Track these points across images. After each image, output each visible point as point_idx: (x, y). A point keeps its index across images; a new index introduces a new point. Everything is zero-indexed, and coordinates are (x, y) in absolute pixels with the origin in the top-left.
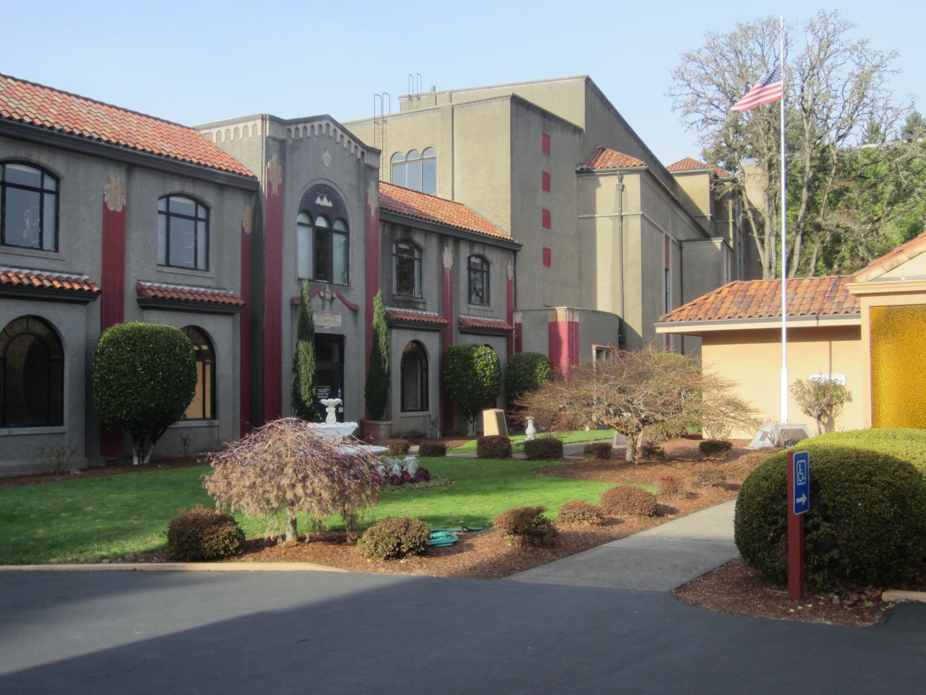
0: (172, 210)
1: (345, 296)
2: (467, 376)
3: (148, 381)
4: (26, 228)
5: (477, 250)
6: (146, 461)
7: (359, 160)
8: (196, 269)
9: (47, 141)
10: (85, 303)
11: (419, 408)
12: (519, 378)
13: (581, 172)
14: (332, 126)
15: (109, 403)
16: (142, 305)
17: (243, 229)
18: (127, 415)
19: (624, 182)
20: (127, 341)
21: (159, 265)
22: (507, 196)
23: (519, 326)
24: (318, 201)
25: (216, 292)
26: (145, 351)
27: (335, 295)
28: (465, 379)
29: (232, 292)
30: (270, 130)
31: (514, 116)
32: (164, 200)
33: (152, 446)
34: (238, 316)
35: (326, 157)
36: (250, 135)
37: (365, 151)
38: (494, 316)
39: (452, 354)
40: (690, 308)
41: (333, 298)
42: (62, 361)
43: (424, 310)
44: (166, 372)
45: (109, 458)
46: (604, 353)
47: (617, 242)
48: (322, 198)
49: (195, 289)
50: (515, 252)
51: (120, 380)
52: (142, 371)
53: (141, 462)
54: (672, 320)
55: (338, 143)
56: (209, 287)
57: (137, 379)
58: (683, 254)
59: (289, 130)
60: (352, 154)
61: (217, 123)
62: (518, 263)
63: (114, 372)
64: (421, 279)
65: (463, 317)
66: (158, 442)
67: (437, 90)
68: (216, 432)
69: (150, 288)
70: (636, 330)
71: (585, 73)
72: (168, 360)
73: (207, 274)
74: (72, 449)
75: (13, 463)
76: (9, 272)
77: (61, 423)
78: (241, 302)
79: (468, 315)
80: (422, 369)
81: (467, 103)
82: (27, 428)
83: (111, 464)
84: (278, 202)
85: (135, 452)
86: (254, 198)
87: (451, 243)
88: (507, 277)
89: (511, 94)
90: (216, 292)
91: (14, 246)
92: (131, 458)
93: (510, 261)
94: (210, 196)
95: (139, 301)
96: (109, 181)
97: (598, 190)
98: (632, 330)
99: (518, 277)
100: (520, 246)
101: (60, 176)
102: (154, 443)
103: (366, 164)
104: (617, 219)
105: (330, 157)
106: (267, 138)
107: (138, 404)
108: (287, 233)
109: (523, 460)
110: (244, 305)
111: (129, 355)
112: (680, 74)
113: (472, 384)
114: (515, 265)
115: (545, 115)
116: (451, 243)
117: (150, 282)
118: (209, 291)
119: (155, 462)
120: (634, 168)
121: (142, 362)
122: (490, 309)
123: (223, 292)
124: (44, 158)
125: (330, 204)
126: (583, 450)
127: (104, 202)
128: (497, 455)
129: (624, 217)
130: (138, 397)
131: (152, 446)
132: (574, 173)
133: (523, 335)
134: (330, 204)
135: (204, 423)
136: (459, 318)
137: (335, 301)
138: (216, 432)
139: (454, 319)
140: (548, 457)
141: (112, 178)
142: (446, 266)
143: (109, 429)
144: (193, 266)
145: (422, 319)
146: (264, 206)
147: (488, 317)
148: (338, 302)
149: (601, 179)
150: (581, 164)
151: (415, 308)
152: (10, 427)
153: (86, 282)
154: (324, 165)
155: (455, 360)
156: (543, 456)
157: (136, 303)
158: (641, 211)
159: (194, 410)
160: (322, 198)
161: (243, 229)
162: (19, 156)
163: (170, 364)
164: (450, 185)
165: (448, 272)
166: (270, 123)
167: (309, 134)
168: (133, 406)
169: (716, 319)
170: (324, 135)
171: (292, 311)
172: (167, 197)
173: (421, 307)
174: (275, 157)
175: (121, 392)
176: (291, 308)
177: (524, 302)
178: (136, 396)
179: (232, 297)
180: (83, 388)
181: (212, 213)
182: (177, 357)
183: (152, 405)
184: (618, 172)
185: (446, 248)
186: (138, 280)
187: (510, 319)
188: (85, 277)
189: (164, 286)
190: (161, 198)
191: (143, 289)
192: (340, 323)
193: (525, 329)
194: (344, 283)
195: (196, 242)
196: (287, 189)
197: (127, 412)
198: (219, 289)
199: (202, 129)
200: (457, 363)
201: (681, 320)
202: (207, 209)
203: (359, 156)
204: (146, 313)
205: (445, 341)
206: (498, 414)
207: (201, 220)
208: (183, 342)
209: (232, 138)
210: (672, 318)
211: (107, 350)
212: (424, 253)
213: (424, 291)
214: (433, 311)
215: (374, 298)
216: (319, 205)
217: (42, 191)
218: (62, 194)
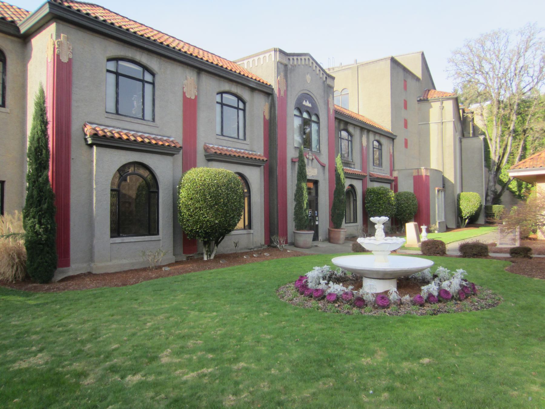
0: (224, 102)
1: (319, 158)
2: (379, 204)
3: (214, 205)
4: (134, 107)
5: (377, 137)
6: (212, 257)
7: (324, 81)
8: (238, 138)
9: (146, 46)
10: (172, 155)
11: (352, 221)
12: (401, 205)
13: (420, 101)
14: (311, 60)
15: (188, 220)
16: (207, 158)
17: (264, 116)
18: (200, 228)
19: (443, 105)
20: (199, 179)
21: (217, 135)
22: (389, 110)
23: (396, 178)
24: (304, 103)
25: (251, 152)
26: (212, 185)
27: (314, 157)
28: (378, 205)
29: (259, 153)
30: (279, 57)
31: (392, 68)
32: (219, 96)
33: (216, 247)
34: (262, 167)
35: (308, 77)
36: (267, 61)
37: (327, 77)
38: (383, 173)
39: (370, 192)
40: (530, 160)
41: (313, 159)
42: (157, 193)
43: (354, 168)
44: (225, 199)
45: (189, 255)
48: (306, 101)
49: (238, 150)
50: (393, 139)
51: (195, 204)
52: (210, 198)
53: (209, 258)
54: (520, 168)
55: (314, 70)
56: (246, 150)
57: (207, 204)
59: (289, 59)
60: (321, 78)
61: (247, 57)
62: (395, 146)
63: (191, 199)
64: (352, 152)
65: (372, 172)
66: (219, 245)
67: (343, 65)
68: (252, 237)
69: (212, 148)
71: (422, 50)
72: (227, 191)
73: (245, 142)
74: (164, 251)
75: (125, 261)
76: (122, 132)
77: (158, 234)
78: (265, 159)
79: (373, 171)
80: (354, 200)
82: (135, 237)
83: (190, 260)
84: (284, 100)
85: (205, 252)
86: (270, 98)
87: (365, 132)
90: (251, 152)
91: (125, 116)
92: (202, 254)
94: (246, 94)
95: (206, 156)
96: (186, 79)
97: (431, 110)
98: (449, 181)
99: (395, 153)
100: (396, 136)
101: (155, 72)
102: (217, 246)
103: (328, 84)
104: (440, 124)
105: (310, 78)
106: (278, 62)
107: (208, 221)
108: (289, 120)
109: (457, 257)
110: (267, 160)
111: (201, 188)
112: (450, 61)
113: (382, 208)
114: (393, 146)
115: (405, 69)
116: (365, 132)
117: (212, 144)
118: (247, 152)
119: (219, 257)
121: (210, 192)
123: (254, 153)
124: (144, 59)
125: (310, 105)
126: (509, 250)
127: (183, 92)
128: (438, 253)
130: (208, 216)
131: (216, 247)
132: (416, 101)
134: (310, 105)
135: (245, 232)
136: (370, 173)
137: (314, 161)
138: (252, 237)
140: (481, 255)
141: (189, 77)
143: (188, 237)
144: (237, 137)
145: (355, 172)
146: (277, 103)
148: (315, 160)
149: (432, 104)
150: (419, 97)
151: (350, 167)
152: (122, 236)
153: (172, 142)
154: (307, 82)
155: (372, 195)
156: (476, 254)
157: (204, 157)
158: (454, 119)
159: (240, 225)
160: (306, 101)
161: (264, 116)
162: (127, 55)
163: (228, 194)
164: (357, 106)
165: (364, 148)
166: (279, 53)
167: (299, 63)
168: (205, 222)
169: (524, 169)
170: (306, 65)
171: (292, 166)
172: (222, 93)
173: (353, 166)
174: (282, 74)
175: (196, 212)
176: (292, 163)
178: (206, 215)
179: (260, 156)
180: (172, 210)
181: (247, 105)
182: (233, 190)
183: (217, 222)
184: (441, 100)
186: (205, 143)
187: (391, 175)
188: (171, 139)
189: (221, 147)
190: (218, 94)
191: (208, 148)
192: (316, 173)
194: (317, 150)
195: (238, 122)
196: (289, 93)
197: (200, 226)
198: (252, 151)
199: (238, 62)
200: (373, 196)
201: (527, 168)
202: (244, 103)
203: (324, 79)
204: (210, 163)
205: (364, 185)
206: (415, 225)
207: (241, 109)
208: (236, 180)
209: (256, 65)
210: (520, 167)
211: (187, 184)
212: (353, 137)
213: (354, 159)
214: (358, 169)
215: (336, 159)
216: (305, 105)
217: (143, 81)
218: (156, 84)
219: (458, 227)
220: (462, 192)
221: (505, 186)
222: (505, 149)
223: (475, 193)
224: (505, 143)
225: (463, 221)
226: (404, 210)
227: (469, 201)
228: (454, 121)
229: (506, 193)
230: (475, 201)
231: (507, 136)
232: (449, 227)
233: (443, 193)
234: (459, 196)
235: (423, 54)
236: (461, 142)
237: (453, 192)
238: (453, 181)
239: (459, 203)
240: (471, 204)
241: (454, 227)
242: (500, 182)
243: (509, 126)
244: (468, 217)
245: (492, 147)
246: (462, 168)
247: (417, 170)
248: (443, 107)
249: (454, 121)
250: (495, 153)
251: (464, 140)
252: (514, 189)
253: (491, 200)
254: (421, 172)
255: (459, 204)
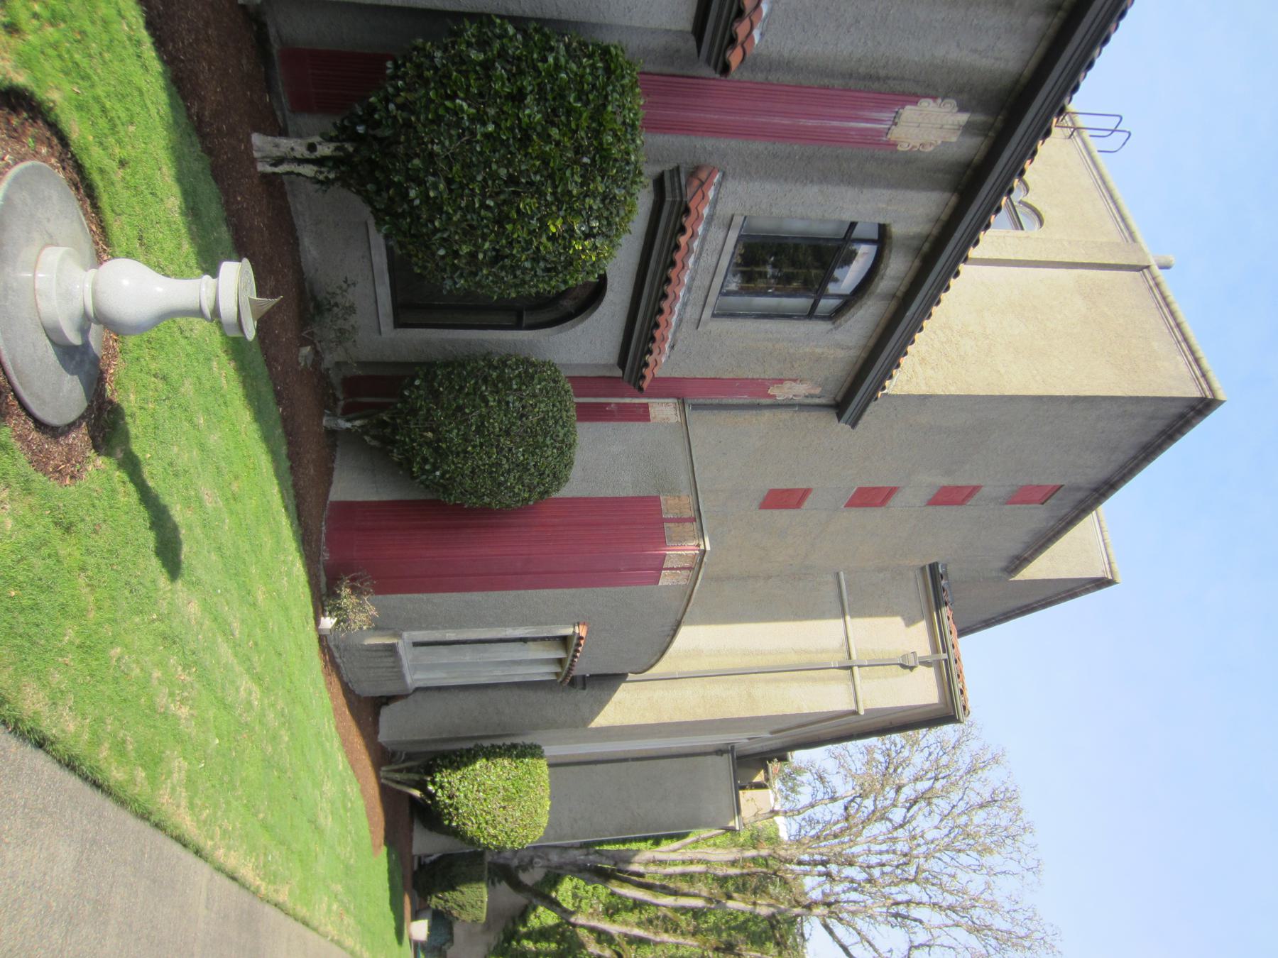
19: (920, 668)
23: (642, 414)
46: (561, 654)
47: (793, 659)
58: (709, 758)
62: (804, 415)
70: (603, 713)
71: (1119, 578)
81: (1164, 298)
88: (781, 381)
89: (1221, 395)
93: (818, 391)
97: (898, 621)
98: (602, 704)
99: (767, 415)
104: (841, 657)
114: (803, 407)
120: (958, 692)
122: (708, 313)
129: (848, 672)
133: (615, 424)
139: (709, 143)
142: (909, 112)
147: (685, 305)
177: (706, 428)
185: (963, 118)
187: (673, 389)
193: (634, 429)
219: (382, 757)
220: (550, 765)
221: (543, 894)
222: (665, 890)
223: (544, 821)
224: (684, 887)
225: (416, 777)
226: (460, 409)
227: (508, 799)
228: (855, 713)
229: (520, 899)
230: (509, 826)
231: (705, 893)
232: (385, 713)
233: (543, 673)
234: (532, 751)
235: (1101, 583)
236: (719, 752)
237: (551, 724)
238: (600, 721)
239: (501, 756)
240: (494, 803)
241: (383, 737)
242: (553, 879)
243: (735, 895)
244: (432, 796)
245: (675, 851)
246: (626, 760)
247: (689, 513)
248: (912, 668)
249: (855, 713)
250: (654, 862)
251: (724, 763)
252: (532, 917)
253: (501, 861)
254: (682, 539)
255: (491, 753)
